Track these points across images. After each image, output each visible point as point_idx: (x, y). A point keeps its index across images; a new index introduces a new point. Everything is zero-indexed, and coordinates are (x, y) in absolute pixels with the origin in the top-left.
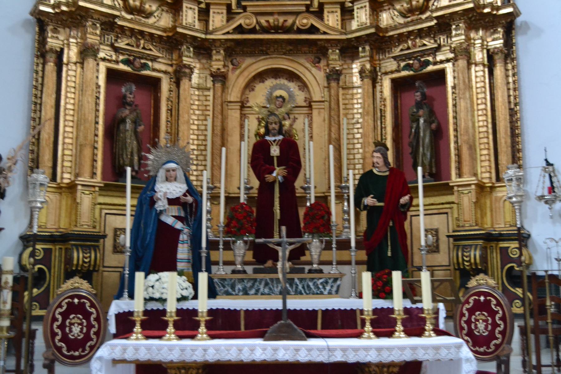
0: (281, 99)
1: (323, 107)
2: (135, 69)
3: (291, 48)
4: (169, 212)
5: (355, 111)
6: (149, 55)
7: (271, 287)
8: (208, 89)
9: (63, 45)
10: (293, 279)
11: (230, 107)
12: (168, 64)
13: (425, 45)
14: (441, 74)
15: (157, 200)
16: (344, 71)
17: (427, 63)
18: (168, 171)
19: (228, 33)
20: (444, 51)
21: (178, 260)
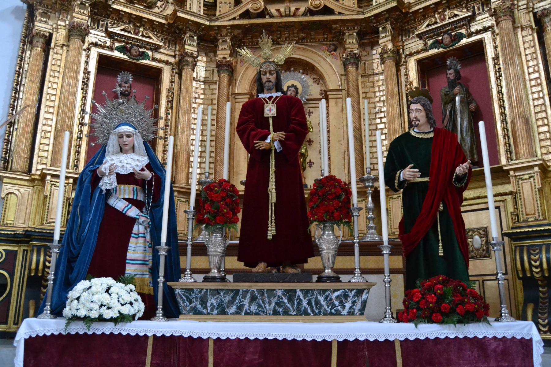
0: (293, 89)
1: (341, 96)
2: (133, 57)
3: (304, 35)
4: (120, 194)
5: (377, 99)
6: (148, 43)
7: (261, 302)
8: (215, 83)
9: (52, 30)
10: (295, 291)
11: (237, 100)
12: (171, 56)
13: (456, 15)
14: (480, 44)
15: (103, 176)
16: (363, 58)
17: (461, 37)
18: (121, 136)
19: (234, 19)
20: (479, 20)
21: (127, 261)
